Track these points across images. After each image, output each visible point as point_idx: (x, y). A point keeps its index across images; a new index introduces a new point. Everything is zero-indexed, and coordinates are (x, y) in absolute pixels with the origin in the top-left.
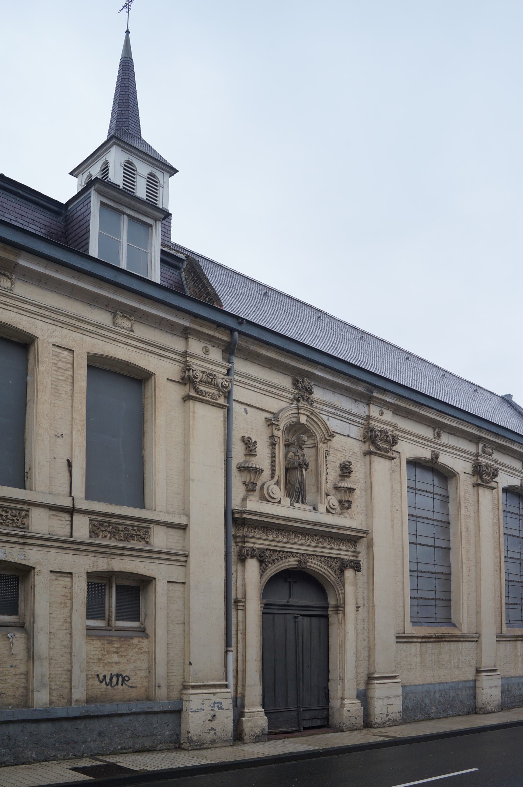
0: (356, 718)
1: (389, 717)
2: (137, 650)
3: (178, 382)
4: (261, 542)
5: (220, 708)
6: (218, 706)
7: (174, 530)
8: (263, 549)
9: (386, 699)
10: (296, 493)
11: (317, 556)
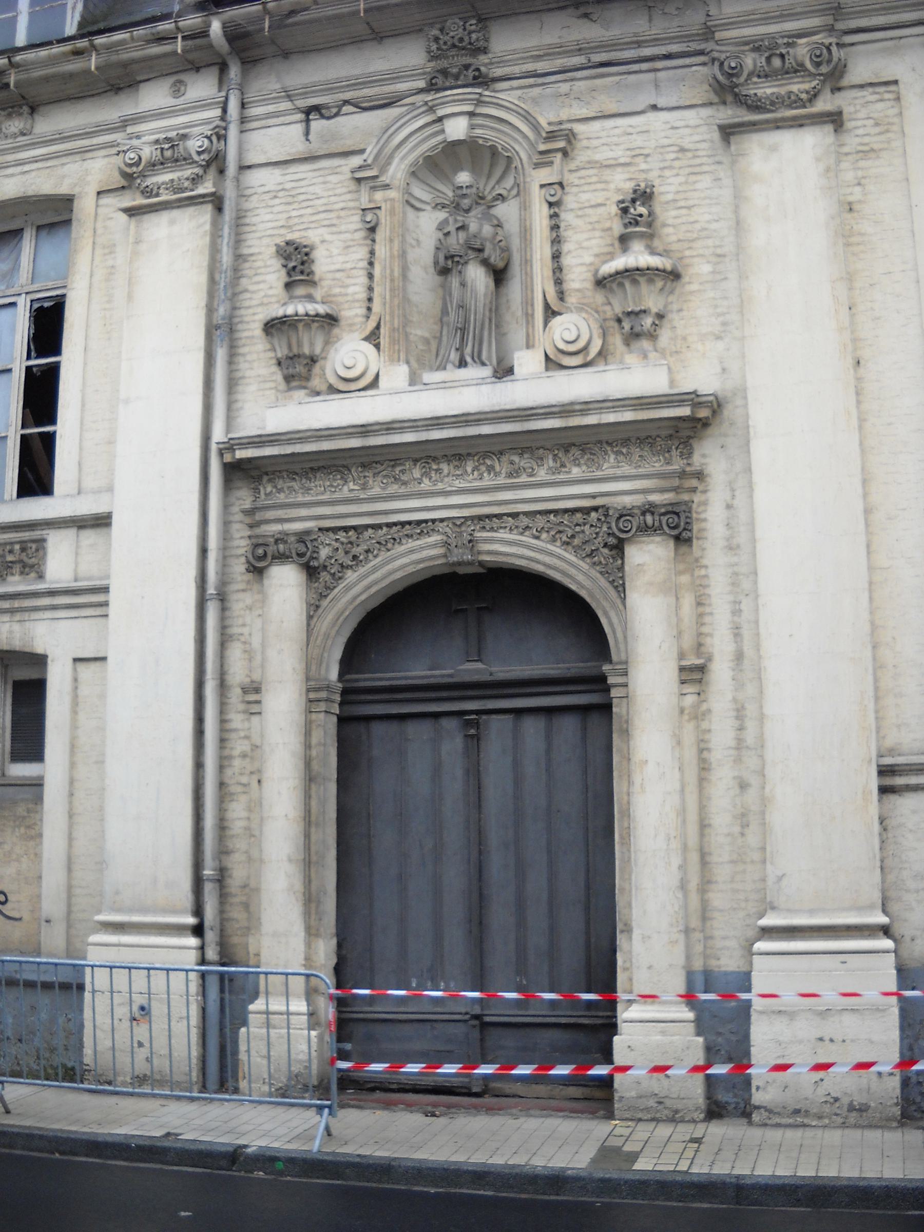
2: (23, 830)
4: (304, 512)
8: (308, 532)
11: (514, 515)
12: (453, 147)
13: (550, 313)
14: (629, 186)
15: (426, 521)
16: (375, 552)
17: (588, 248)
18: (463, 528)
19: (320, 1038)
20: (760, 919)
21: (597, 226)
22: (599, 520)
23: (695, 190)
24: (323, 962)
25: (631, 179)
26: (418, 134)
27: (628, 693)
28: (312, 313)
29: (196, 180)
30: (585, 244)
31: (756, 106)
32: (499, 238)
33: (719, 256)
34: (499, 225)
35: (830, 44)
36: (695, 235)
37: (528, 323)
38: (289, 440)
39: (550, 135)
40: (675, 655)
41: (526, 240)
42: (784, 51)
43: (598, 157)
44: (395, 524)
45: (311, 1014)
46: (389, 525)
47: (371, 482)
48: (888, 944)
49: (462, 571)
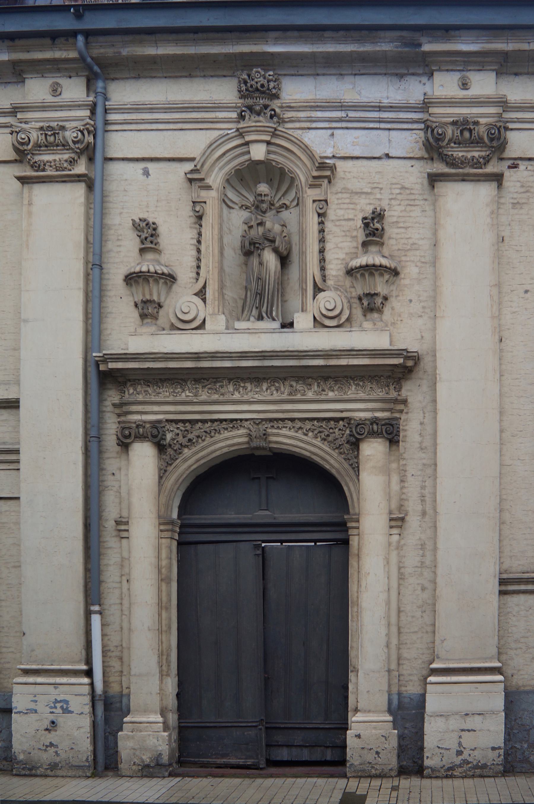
0: (377, 753)
1: (465, 756)
3: (16, 161)
4: (156, 408)
5: (66, 711)
6: (62, 707)
7: (9, 411)
8: (159, 421)
9: (457, 717)
10: (263, 300)
11: (292, 420)
12: (255, 164)
13: (317, 290)
14: (369, 209)
15: (236, 420)
16: (203, 438)
17: (341, 248)
18: (260, 426)
19: (170, 736)
20: (431, 664)
21: (348, 234)
22: (344, 426)
23: (410, 216)
24: (171, 691)
25: (370, 204)
26: (232, 152)
27: (359, 533)
28: (160, 272)
29: (72, 162)
30: (339, 245)
31: (451, 162)
32: (284, 234)
33: (423, 263)
34: (284, 225)
35: (500, 126)
36: (409, 247)
37: (303, 295)
38: (145, 358)
39: (321, 165)
40: (387, 511)
41: (303, 237)
42: (472, 127)
43: (349, 186)
44: (216, 420)
45: (164, 723)
46: (213, 421)
47: (200, 391)
48: (500, 678)
49: (257, 453)
